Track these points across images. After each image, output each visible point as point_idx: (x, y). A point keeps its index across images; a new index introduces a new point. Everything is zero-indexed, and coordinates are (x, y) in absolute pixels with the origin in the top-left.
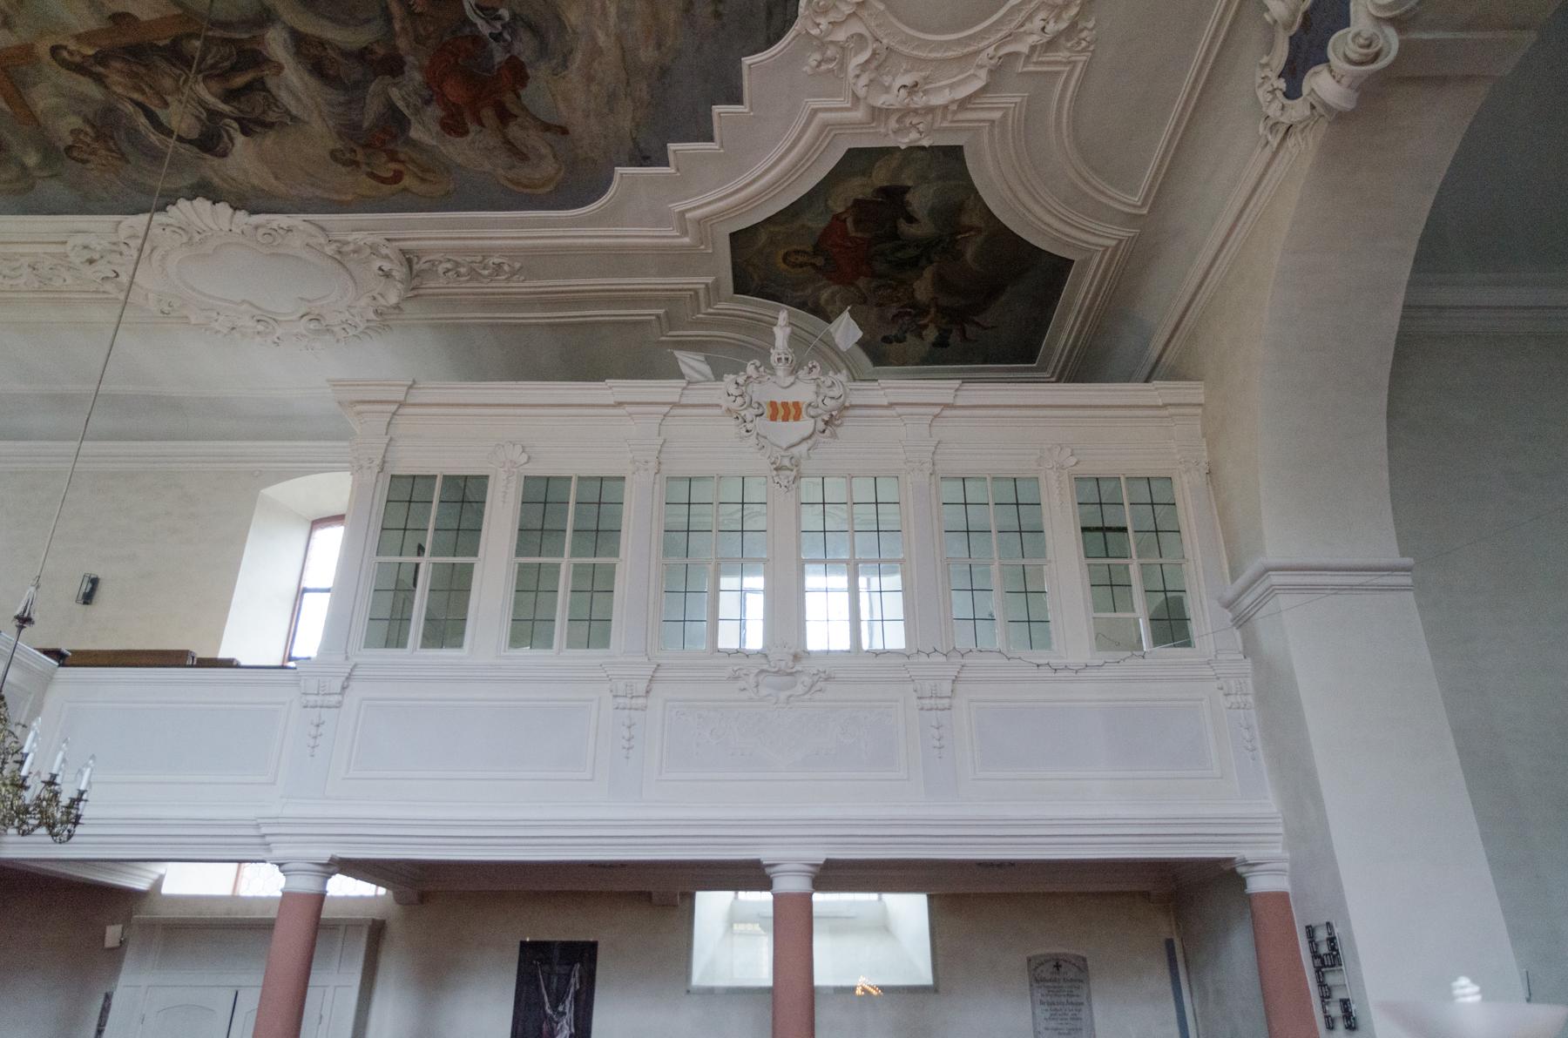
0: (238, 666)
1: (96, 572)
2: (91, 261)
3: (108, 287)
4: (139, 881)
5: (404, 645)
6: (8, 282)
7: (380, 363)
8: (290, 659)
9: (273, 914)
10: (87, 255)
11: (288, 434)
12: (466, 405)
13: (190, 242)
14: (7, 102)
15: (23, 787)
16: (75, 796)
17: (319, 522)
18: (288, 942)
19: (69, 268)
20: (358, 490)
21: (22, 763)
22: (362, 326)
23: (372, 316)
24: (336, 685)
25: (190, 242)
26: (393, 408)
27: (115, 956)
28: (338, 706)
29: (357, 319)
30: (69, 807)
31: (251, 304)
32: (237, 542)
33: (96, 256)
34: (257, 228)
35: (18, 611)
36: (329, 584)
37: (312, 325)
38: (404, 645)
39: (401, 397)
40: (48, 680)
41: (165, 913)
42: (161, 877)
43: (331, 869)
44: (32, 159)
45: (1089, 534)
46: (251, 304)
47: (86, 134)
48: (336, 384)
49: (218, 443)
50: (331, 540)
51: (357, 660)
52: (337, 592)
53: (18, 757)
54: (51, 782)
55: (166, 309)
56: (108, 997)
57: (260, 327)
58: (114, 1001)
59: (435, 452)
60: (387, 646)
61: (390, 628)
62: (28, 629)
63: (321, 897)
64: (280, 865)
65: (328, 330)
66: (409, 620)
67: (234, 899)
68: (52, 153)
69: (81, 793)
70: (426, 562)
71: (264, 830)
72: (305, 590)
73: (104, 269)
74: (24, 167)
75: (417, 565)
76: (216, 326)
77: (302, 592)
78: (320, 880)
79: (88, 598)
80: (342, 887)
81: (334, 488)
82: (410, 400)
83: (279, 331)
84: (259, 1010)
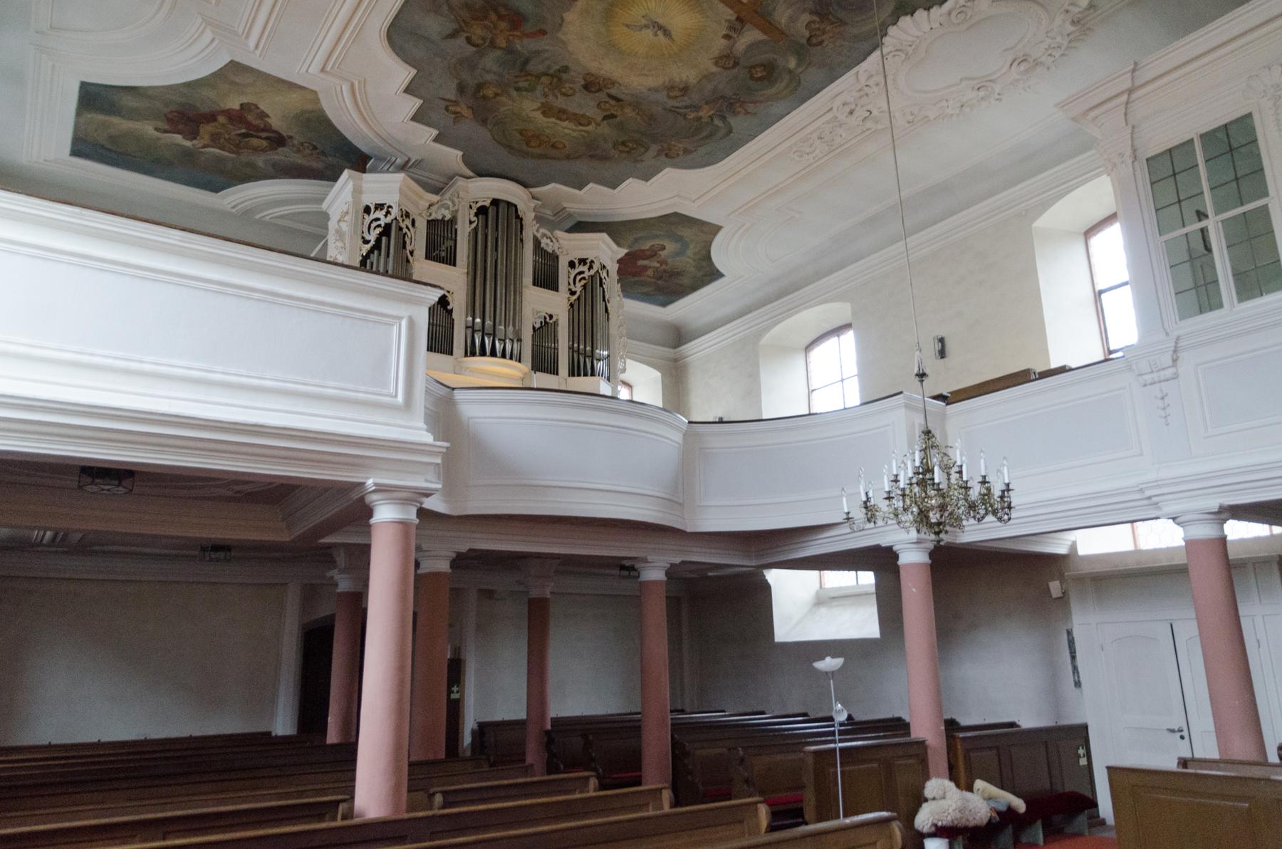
0: (1072, 370)
1: (941, 334)
2: (851, 113)
3: (869, 124)
4: (1059, 547)
5: (1221, 306)
6: (811, 157)
7: (1096, 66)
8: (1111, 352)
9: (1181, 560)
10: (847, 109)
11: (1037, 169)
12: (1161, 76)
13: (908, 57)
14: (765, 33)
15: (967, 488)
16: (1004, 487)
17: (1089, 232)
18: (1208, 578)
19: (841, 126)
20: (1121, 190)
21: (960, 472)
22: (1065, 43)
23: (1070, 28)
24: (1167, 359)
25: (908, 57)
26: (1125, 97)
27: (1064, 600)
28: (1176, 377)
29: (1059, 39)
30: (1002, 497)
31: (967, 79)
32: (1029, 274)
33: (853, 107)
34: (949, 14)
35: (916, 371)
36: (1125, 277)
37: (1022, 68)
38: (1221, 306)
39: (1128, 84)
40: (943, 417)
41: (1087, 569)
42: (1074, 544)
43: (1223, 516)
44: (792, 63)
45: (1222, 135)
46: (967, 79)
47: (814, 22)
48: (1062, 105)
49: (985, 203)
50: (1113, 237)
51: (1176, 333)
52: (1136, 282)
53: (957, 469)
54: (984, 482)
55: (910, 118)
56: (1069, 633)
57: (982, 93)
58: (1075, 634)
59: (1183, 117)
60: (1201, 312)
61: (1201, 294)
62: (926, 381)
63: (1223, 540)
64: (1174, 519)
65: (1037, 63)
66: (1216, 281)
67: (1137, 552)
68: (801, 51)
69: (1008, 485)
70: (1213, 225)
71: (1148, 493)
72: (1101, 292)
73: (860, 113)
74: (790, 72)
75: (1203, 231)
76: (949, 111)
77: (1098, 295)
78: (1215, 526)
79: (942, 354)
80: (1237, 530)
81: (1098, 193)
82: (1138, 82)
83: (997, 88)
84: (1201, 633)
